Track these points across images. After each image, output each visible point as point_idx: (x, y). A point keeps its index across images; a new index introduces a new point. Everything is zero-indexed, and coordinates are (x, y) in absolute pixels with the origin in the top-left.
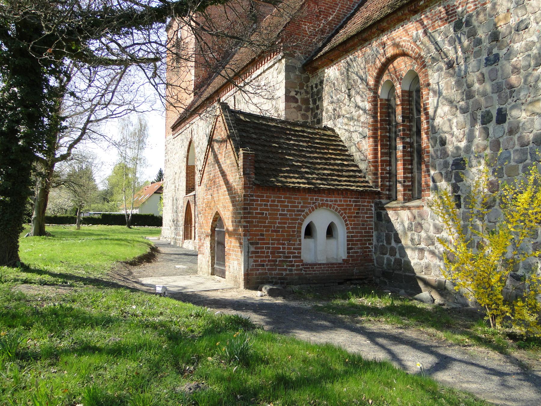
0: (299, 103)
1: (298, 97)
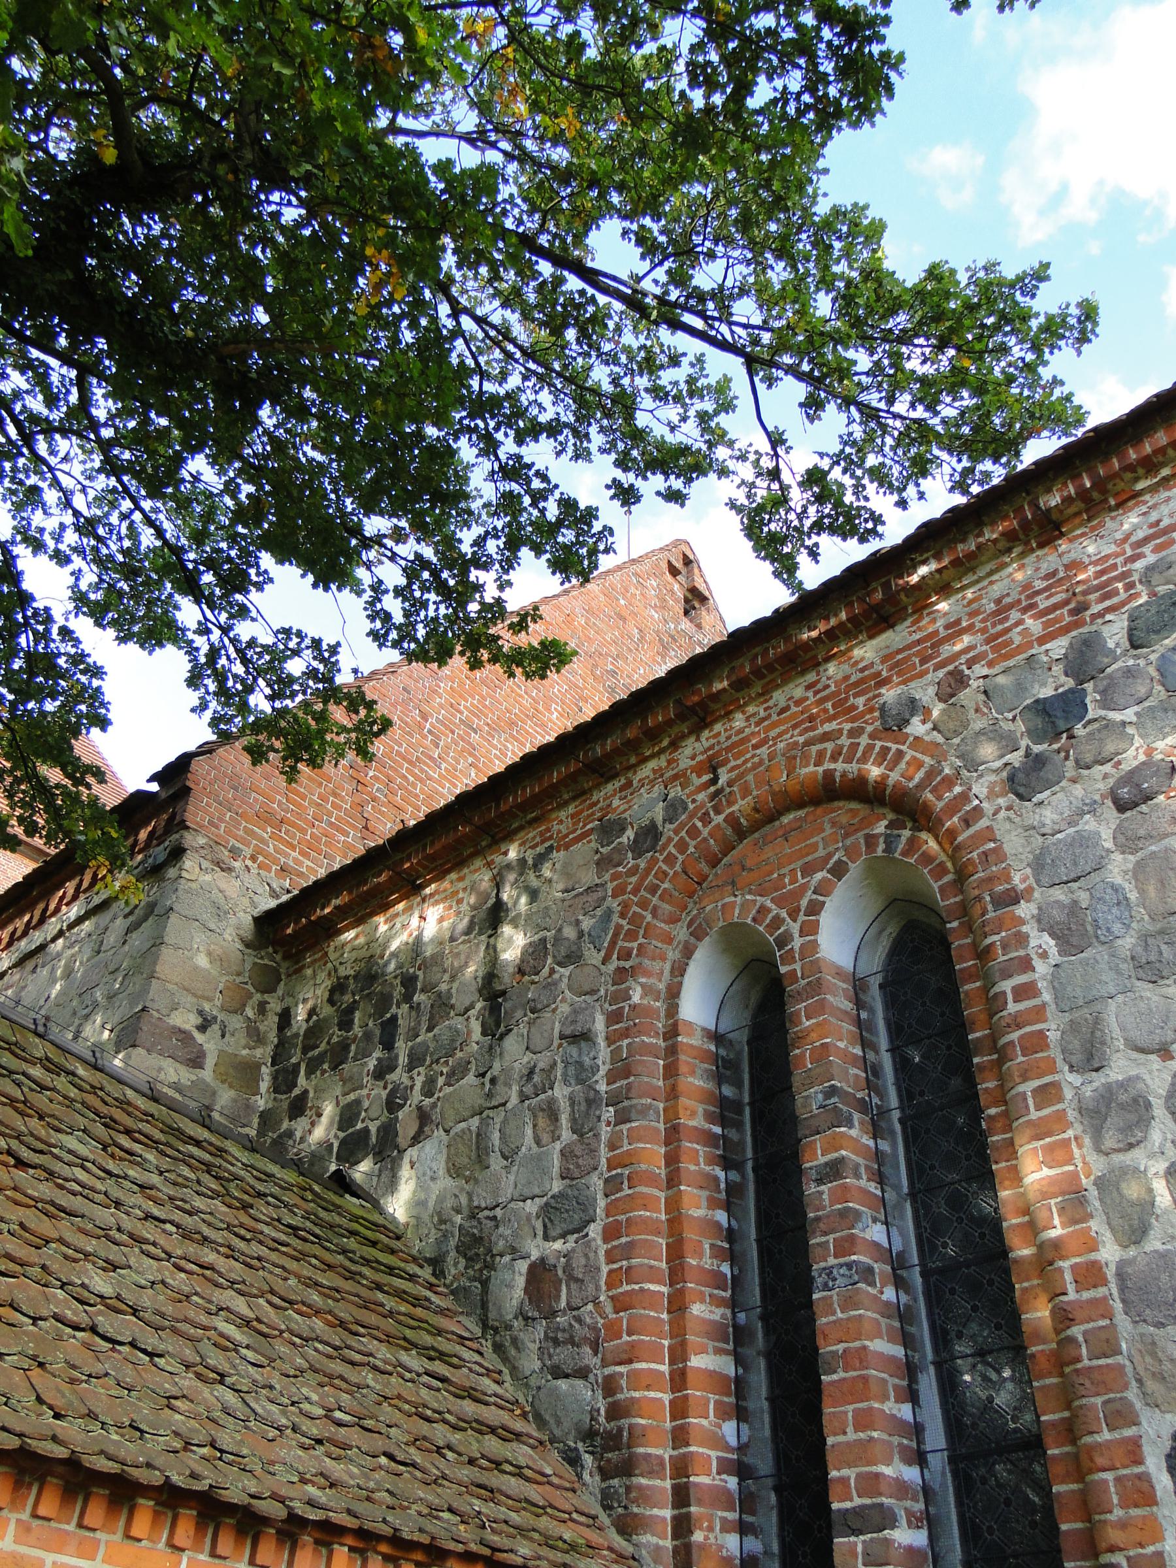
0: (207, 1074)
1: (209, 1042)
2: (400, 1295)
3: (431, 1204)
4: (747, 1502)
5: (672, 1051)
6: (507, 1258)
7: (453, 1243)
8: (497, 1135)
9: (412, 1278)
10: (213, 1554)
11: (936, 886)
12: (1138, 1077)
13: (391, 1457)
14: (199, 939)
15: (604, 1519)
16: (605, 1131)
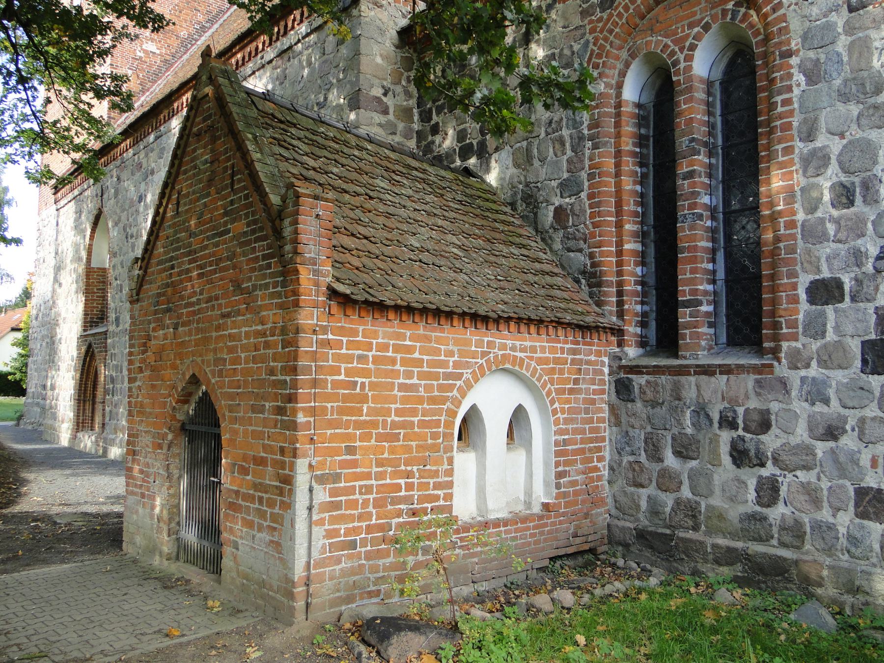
0: (391, 117)
1: (388, 101)
2: (503, 222)
3: (507, 179)
4: (644, 294)
5: (618, 115)
6: (544, 205)
7: (519, 197)
8: (536, 150)
9: (505, 213)
10: (476, 328)
11: (754, 41)
12: (828, 146)
13: (519, 290)
14: (376, 49)
15: (590, 301)
16: (587, 152)
